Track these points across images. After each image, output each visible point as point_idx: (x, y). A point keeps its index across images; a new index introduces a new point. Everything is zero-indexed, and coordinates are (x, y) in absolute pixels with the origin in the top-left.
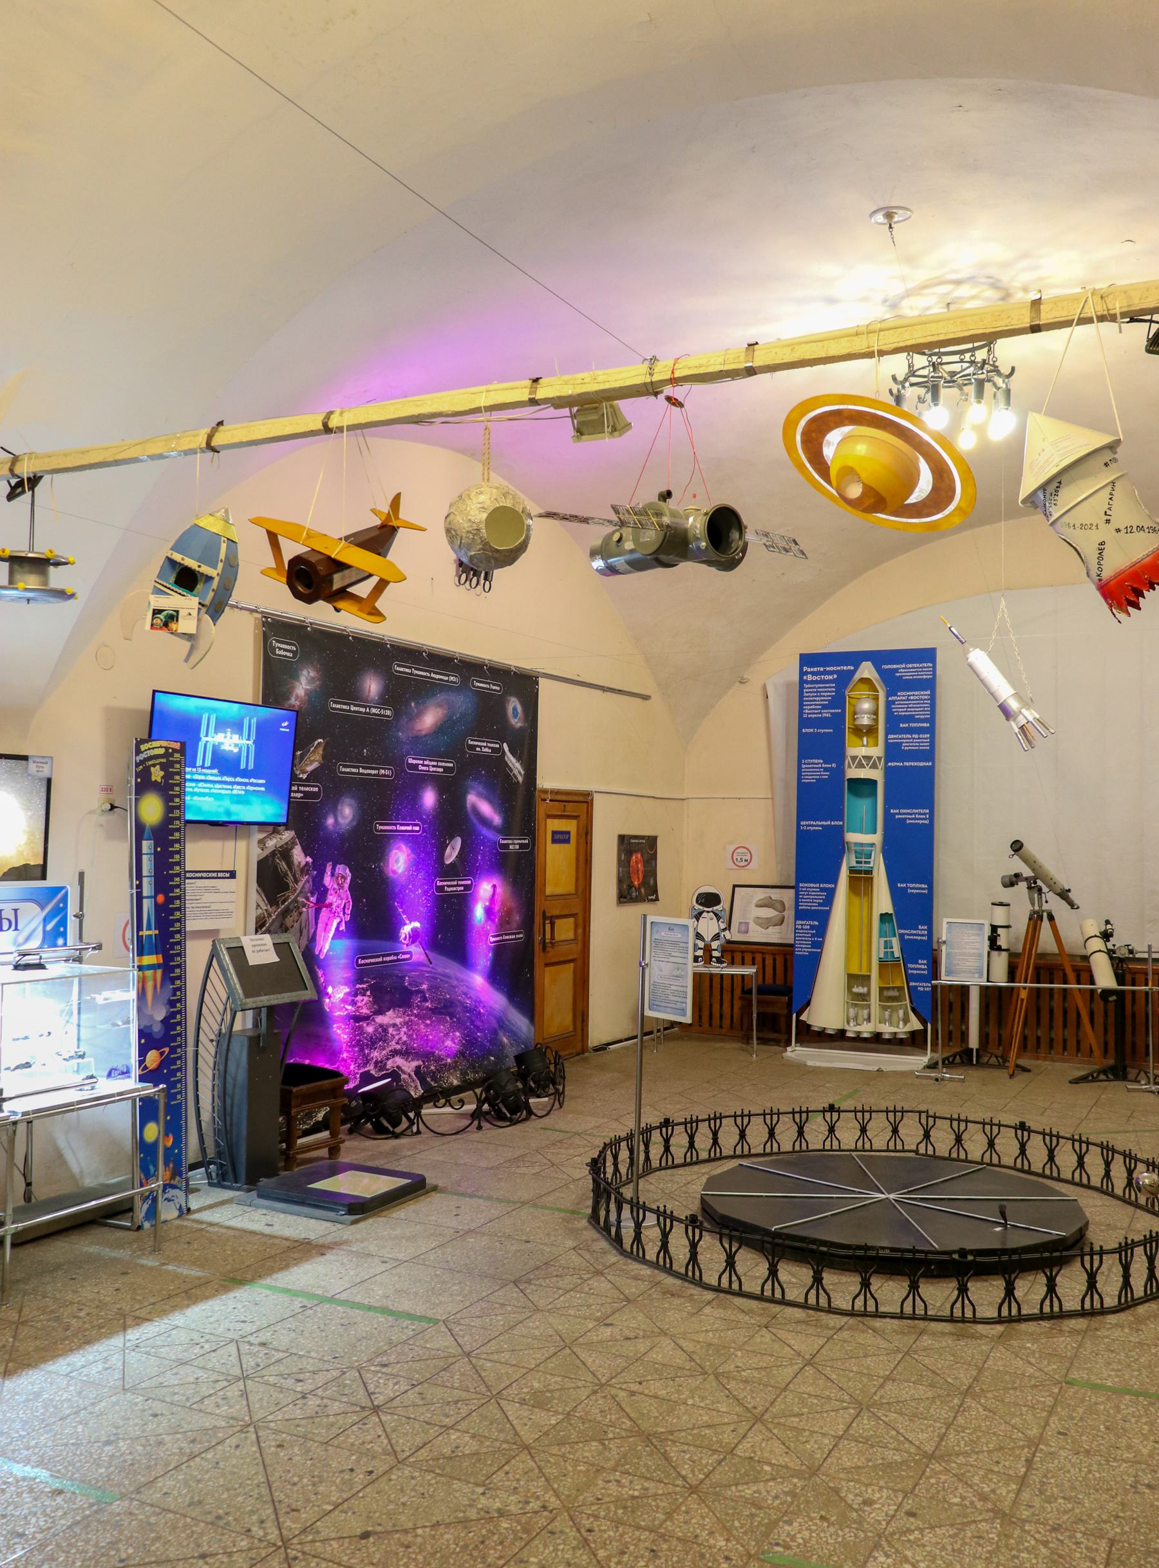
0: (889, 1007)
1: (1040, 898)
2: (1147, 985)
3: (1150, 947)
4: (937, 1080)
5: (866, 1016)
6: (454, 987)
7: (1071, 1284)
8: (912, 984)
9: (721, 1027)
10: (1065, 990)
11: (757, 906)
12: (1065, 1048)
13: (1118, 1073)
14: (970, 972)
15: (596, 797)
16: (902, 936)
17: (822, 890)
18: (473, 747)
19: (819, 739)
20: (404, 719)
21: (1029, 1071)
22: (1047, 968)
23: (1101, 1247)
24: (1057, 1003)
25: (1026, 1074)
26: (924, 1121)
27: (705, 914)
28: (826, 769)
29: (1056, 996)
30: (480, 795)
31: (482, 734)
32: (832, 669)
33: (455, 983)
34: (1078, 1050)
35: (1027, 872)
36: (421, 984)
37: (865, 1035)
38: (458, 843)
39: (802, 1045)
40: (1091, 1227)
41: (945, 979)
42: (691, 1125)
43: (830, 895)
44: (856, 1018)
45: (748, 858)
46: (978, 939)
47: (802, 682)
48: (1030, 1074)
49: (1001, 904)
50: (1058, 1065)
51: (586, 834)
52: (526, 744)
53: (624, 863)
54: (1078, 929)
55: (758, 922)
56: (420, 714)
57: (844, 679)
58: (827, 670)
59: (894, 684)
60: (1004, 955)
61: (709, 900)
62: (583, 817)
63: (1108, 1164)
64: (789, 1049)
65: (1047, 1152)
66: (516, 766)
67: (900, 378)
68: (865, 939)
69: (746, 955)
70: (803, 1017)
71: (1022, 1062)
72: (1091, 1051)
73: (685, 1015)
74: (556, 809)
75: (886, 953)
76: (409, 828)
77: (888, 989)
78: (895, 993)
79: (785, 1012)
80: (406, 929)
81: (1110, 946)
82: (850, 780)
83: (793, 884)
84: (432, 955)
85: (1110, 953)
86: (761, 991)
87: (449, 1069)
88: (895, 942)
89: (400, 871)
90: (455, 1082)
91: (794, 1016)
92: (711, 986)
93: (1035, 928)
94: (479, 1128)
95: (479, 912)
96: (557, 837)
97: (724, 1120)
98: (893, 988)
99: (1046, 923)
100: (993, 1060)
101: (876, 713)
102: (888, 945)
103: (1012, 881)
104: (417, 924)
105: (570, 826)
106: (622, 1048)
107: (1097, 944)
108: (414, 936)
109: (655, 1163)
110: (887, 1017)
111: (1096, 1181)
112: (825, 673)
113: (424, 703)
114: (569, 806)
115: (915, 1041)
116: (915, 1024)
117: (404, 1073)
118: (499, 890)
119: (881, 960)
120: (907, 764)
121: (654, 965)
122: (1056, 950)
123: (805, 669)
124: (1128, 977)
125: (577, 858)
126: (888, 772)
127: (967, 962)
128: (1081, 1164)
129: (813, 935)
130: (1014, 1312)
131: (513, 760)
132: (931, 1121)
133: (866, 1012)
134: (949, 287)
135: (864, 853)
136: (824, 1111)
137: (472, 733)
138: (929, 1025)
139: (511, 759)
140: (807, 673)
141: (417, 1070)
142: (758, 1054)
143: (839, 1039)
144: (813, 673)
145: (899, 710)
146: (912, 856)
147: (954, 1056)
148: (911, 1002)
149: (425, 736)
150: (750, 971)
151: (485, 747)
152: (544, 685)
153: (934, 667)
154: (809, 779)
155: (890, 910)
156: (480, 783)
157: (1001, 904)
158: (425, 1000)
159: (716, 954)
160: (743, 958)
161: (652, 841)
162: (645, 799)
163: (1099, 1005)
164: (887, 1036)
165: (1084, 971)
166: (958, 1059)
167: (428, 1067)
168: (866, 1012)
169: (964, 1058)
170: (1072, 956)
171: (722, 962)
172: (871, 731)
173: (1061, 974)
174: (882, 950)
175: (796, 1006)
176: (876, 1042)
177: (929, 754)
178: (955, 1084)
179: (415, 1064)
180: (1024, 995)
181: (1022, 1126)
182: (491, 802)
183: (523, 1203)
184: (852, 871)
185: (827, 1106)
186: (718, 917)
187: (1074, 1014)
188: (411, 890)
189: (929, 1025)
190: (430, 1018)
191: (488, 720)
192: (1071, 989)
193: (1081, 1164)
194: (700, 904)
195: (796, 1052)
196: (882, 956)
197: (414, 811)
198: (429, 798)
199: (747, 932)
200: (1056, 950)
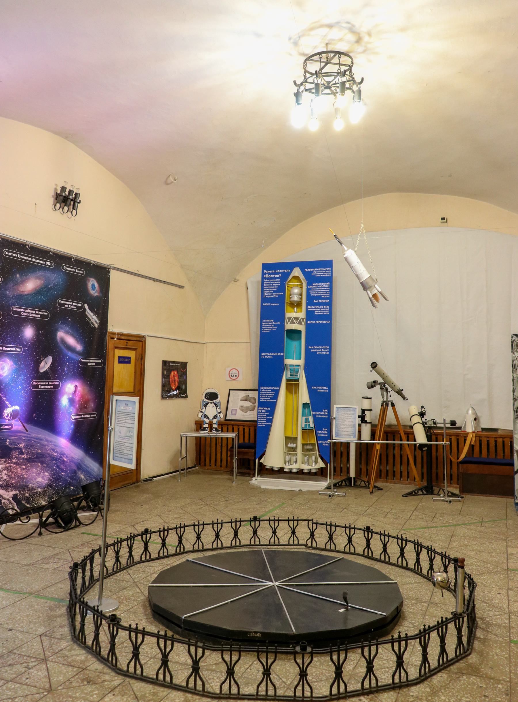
0: (308, 455)
1: (387, 394)
2: (443, 441)
3: (444, 420)
4: (330, 496)
5: (295, 460)
6: (45, 446)
7: (385, 658)
8: (319, 442)
9: (221, 466)
10: (401, 444)
11: (241, 400)
12: (401, 476)
13: (429, 490)
14: (349, 435)
15: (148, 340)
16: (314, 416)
17: (272, 390)
18: (63, 305)
19: (272, 308)
20: (11, 284)
21: (382, 489)
22: (391, 433)
23: (406, 634)
24: (397, 452)
25: (380, 491)
26: (310, 526)
27: (209, 404)
28: (275, 325)
29: (396, 448)
30: (67, 333)
31: (69, 297)
32: (279, 271)
33: (46, 443)
34: (408, 477)
35: (380, 380)
36: (19, 444)
37: (294, 471)
38: (49, 360)
39: (261, 476)
40: (405, 603)
41: (335, 439)
42: (164, 532)
43: (276, 394)
44: (290, 461)
45: (237, 374)
46: (353, 416)
47: (263, 278)
48: (382, 491)
49: (367, 398)
50: (397, 486)
51: (141, 360)
52: (101, 306)
53: (165, 376)
54: (406, 411)
55: (241, 410)
56: (23, 282)
57: (285, 277)
58: (277, 273)
59: (311, 279)
60: (369, 426)
61: (212, 396)
62: (139, 350)
63: (418, 554)
64: (254, 479)
65: (382, 546)
66: (93, 318)
67: (298, 83)
68: (295, 417)
69: (234, 427)
70: (262, 461)
71: (378, 484)
72: (415, 478)
73: (131, 464)
74: (122, 344)
75: (306, 425)
76: (13, 349)
77: (307, 445)
78: (311, 447)
79: (253, 458)
80: (8, 411)
81: (424, 420)
82: (287, 331)
83: (257, 388)
84: (27, 426)
85: (424, 424)
86: (240, 446)
87: (40, 495)
88: (311, 419)
89: (5, 375)
90: (44, 503)
91: (257, 460)
92: (216, 444)
93: (384, 411)
94: (40, 534)
95: (64, 401)
96: (122, 360)
97: (186, 528)
98: (310, 444)
99: (390, 408)
100: (363, 484)
101: (301, 295)
102: (307, 420)
103: (372, 385)
104: (17, 408)
105: (131, 354)
106: (162, 479)
107: (417, 419)
108: (14, 415)
109: (137, 558)
110: (306, 460)
111: (411, 565)
112: (275, 273)
113: (26, 275)
114: (130, 343)
115: (321, 473)
116: (321, 464)
117: (4, 499)
118: (79, 388)
119: (303, 429)
120: (317, 322)
121: (117, 428)
122: (396, 423)
123: (265, 271)
124: (434, 437)
125: (135, 373)
126: (308, 326)
127: (346, 428)
128: (402, 553)
129: (267, 416)
130: (342, 689)
131: (92, 314)
132: (315, 526)
133: (295, 458)
134: (325, 30)
135: (294, 370)
136: (250, 521)
137: (62, 297)
138: (329, 465)
139: (90, 314)
140: (266, 274)
141: (15, 497)
142: (236, 482)
143: (280, 473)
144: (269, 274)
145: (314, 293)
146: (320, 371)
147: (342, 482)
148: (319, 452)
149: (26, 295)
150: (233, 435)
151: (71, 305)
152: (113, 274)
153: (332, 270)
154: (266, 330)
155: (308, 401)
156: (68, 325)
157: (367, 398)
158: (22, 453)
159: (215, 426)
160: (233, 428)
161: (184, 365)
162: (181, 342)
163: (419, 453)
164: (306, 471)
165: (410, 435)
166: (344, 484)
167: (23, 495)
168: (295, 458)
169: (348, 483)
170: (405, 426)
171: (219, 431)
172: (299, 304)
173: (399, 436)
174: (304, 423)
175: (258, 455)
176: (300, 474)
177: (329, 317)
178: (340, 498)
179: (13, 493)
180: (378, 447)
181: (368, 529)
182: (72, 335)
183: (31, 594)
184: (288, 380)
185: (252, 517)
186: (216, 406)
187: (406, 458)
188: (13, 387)
189: (329, 465)
190: (25, 465)
191: (75, 288)
192: (404, 444)
193: (402, 553)
194: (207, 399)
195: (258, 481)
196: (304, 426)
197: (17, 339)
198: (29, 332)
199: (236, 415)
200: (396, 423)
